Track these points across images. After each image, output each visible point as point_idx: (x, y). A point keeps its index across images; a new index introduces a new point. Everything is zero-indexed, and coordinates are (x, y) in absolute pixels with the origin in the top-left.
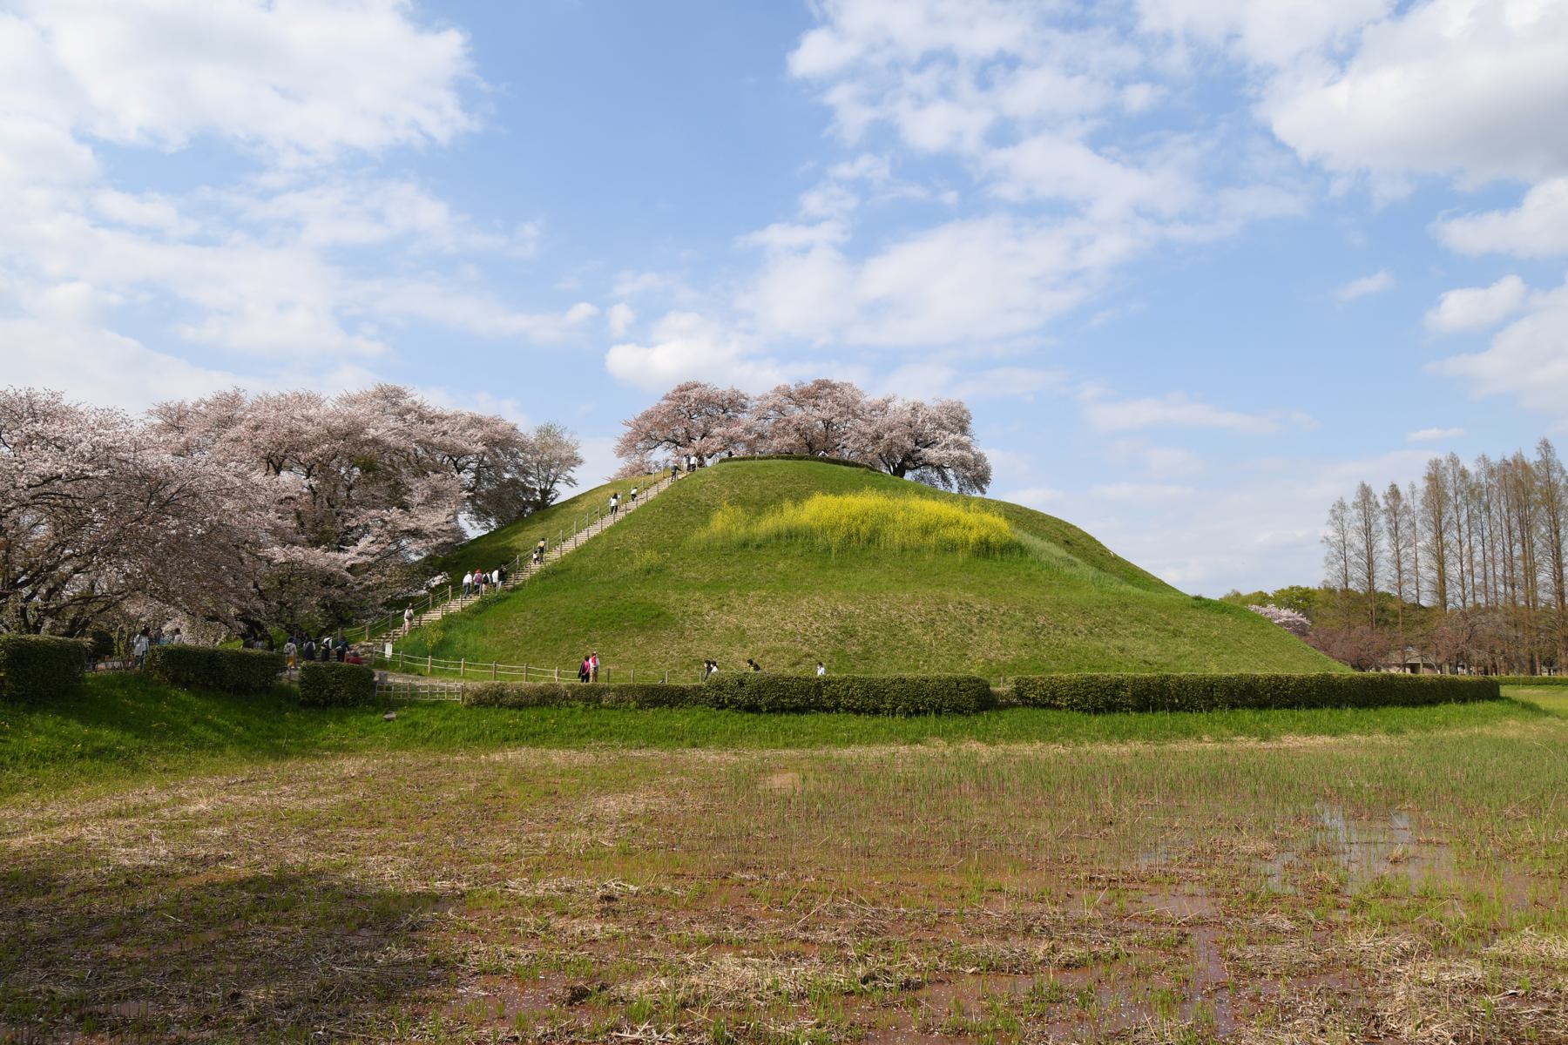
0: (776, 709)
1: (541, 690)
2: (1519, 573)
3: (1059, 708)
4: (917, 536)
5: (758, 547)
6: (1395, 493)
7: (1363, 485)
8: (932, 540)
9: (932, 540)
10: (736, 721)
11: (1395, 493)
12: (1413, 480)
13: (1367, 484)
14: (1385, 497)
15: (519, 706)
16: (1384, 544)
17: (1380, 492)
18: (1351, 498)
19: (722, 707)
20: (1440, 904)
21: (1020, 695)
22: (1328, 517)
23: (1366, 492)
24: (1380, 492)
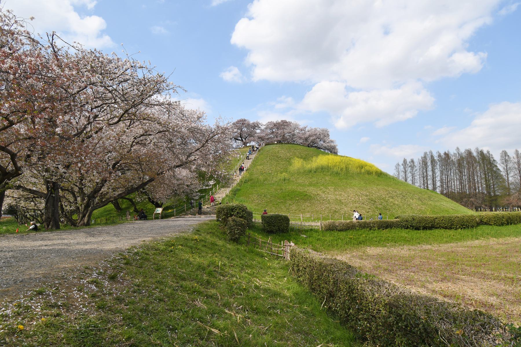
0: (425, 228)
1: (348, 224)
2: (31, 195)
3: (491, 225)
4: (358, 170)
5: (315, 172)
6: (412, 161)
7: (405, 159)
8: (363, 170)
9: (363, 170)
10: (415, 234)
11: (505, 154)
12: (417, 158)
13: (406, 159)
14: (409, 162)
15: (340, 230)
16: (430, 173)
17: (408, 160)
18: (401, 162)
19: (407, 228)
20: (469, 298)
21: (481, 221)
22: (394, 168)
23: (405, 161)
24: (408, 160)
